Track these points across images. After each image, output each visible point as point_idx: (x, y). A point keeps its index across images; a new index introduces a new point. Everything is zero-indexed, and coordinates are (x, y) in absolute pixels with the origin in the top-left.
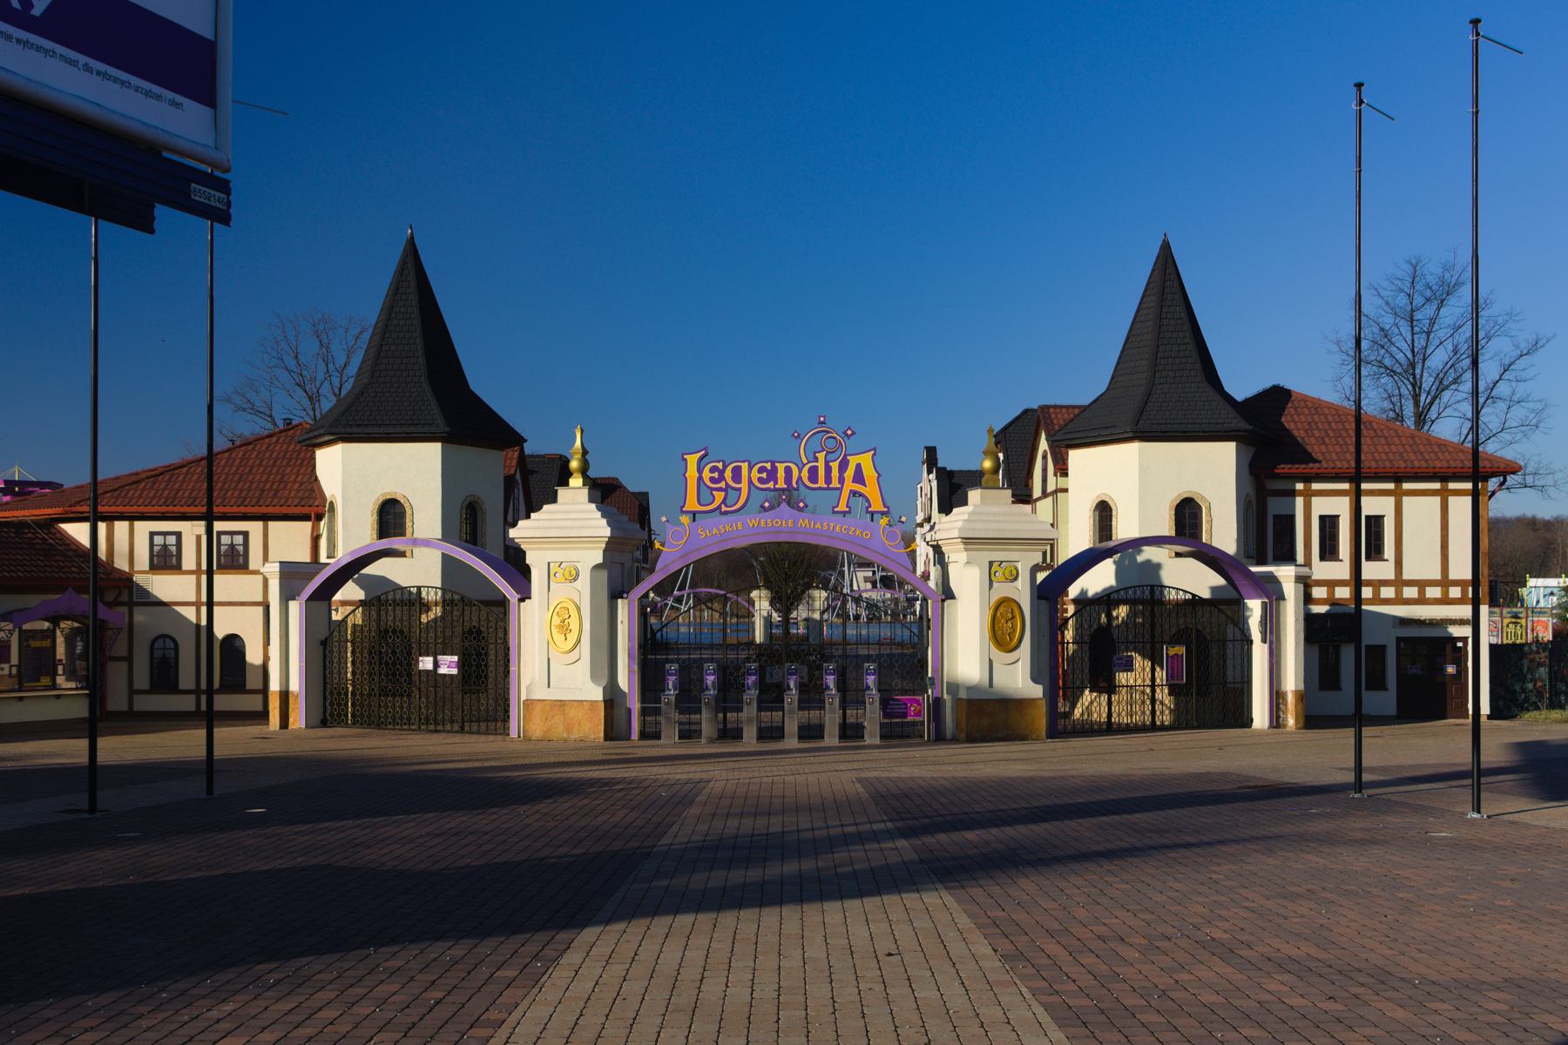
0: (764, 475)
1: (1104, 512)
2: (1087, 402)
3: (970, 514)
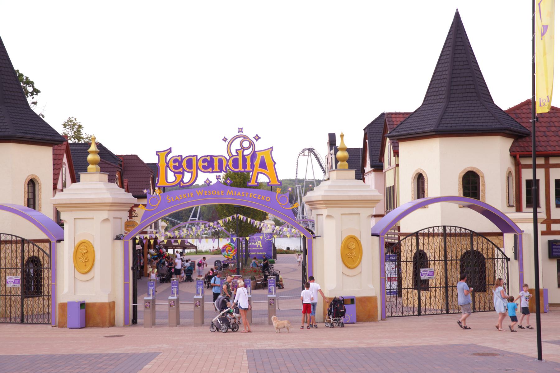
0: (206, 164)
1: (420, 179)
2: (413, 111)
3: (329, 186)
